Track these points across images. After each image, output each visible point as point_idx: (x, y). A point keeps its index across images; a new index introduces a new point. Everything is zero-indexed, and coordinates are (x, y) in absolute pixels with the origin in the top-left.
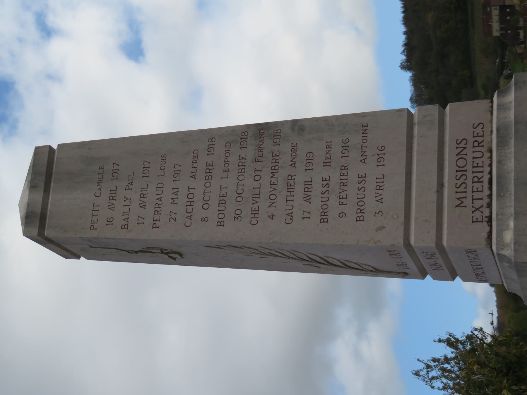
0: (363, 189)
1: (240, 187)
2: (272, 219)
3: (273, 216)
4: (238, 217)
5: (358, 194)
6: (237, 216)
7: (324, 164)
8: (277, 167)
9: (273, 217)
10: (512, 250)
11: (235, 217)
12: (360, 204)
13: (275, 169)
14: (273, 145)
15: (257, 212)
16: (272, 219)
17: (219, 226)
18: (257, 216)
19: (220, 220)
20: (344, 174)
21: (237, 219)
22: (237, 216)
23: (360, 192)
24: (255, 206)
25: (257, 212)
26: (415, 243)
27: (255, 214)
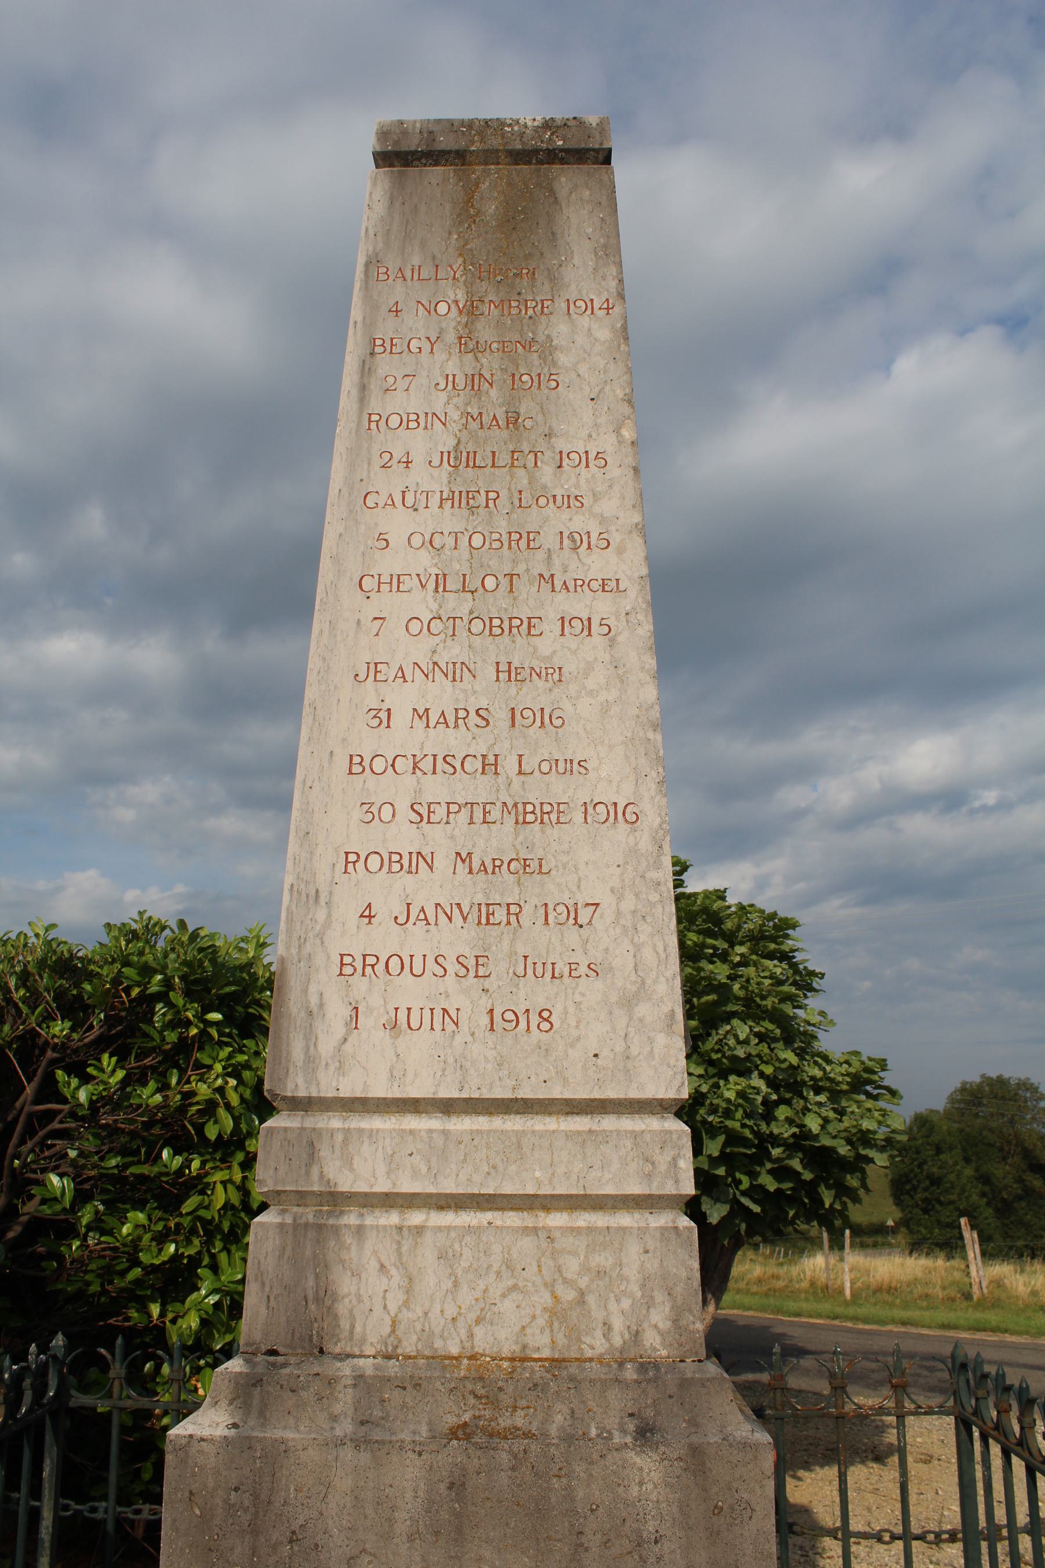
0: (440, 971)
1: (450, 541)
2: (362, 916)
3: (370, 917)
5: (432, 1029)
6: (375, 809)
7: (501, 679)
8: (499, 631)
9: (366, 917)
10: (336, 559)
12: (394, 963)
13: (525, 813)
14: (563, 618)
15: (395, 588)
16: (362, 916)
17: (347, 858)
18: (386, 587)
19: (366, 763)
20: (493, 914)
21: (375, 717)
22: (375, 809)
23: (430, 960)
24: (407, 583)
26: (260, 1223)
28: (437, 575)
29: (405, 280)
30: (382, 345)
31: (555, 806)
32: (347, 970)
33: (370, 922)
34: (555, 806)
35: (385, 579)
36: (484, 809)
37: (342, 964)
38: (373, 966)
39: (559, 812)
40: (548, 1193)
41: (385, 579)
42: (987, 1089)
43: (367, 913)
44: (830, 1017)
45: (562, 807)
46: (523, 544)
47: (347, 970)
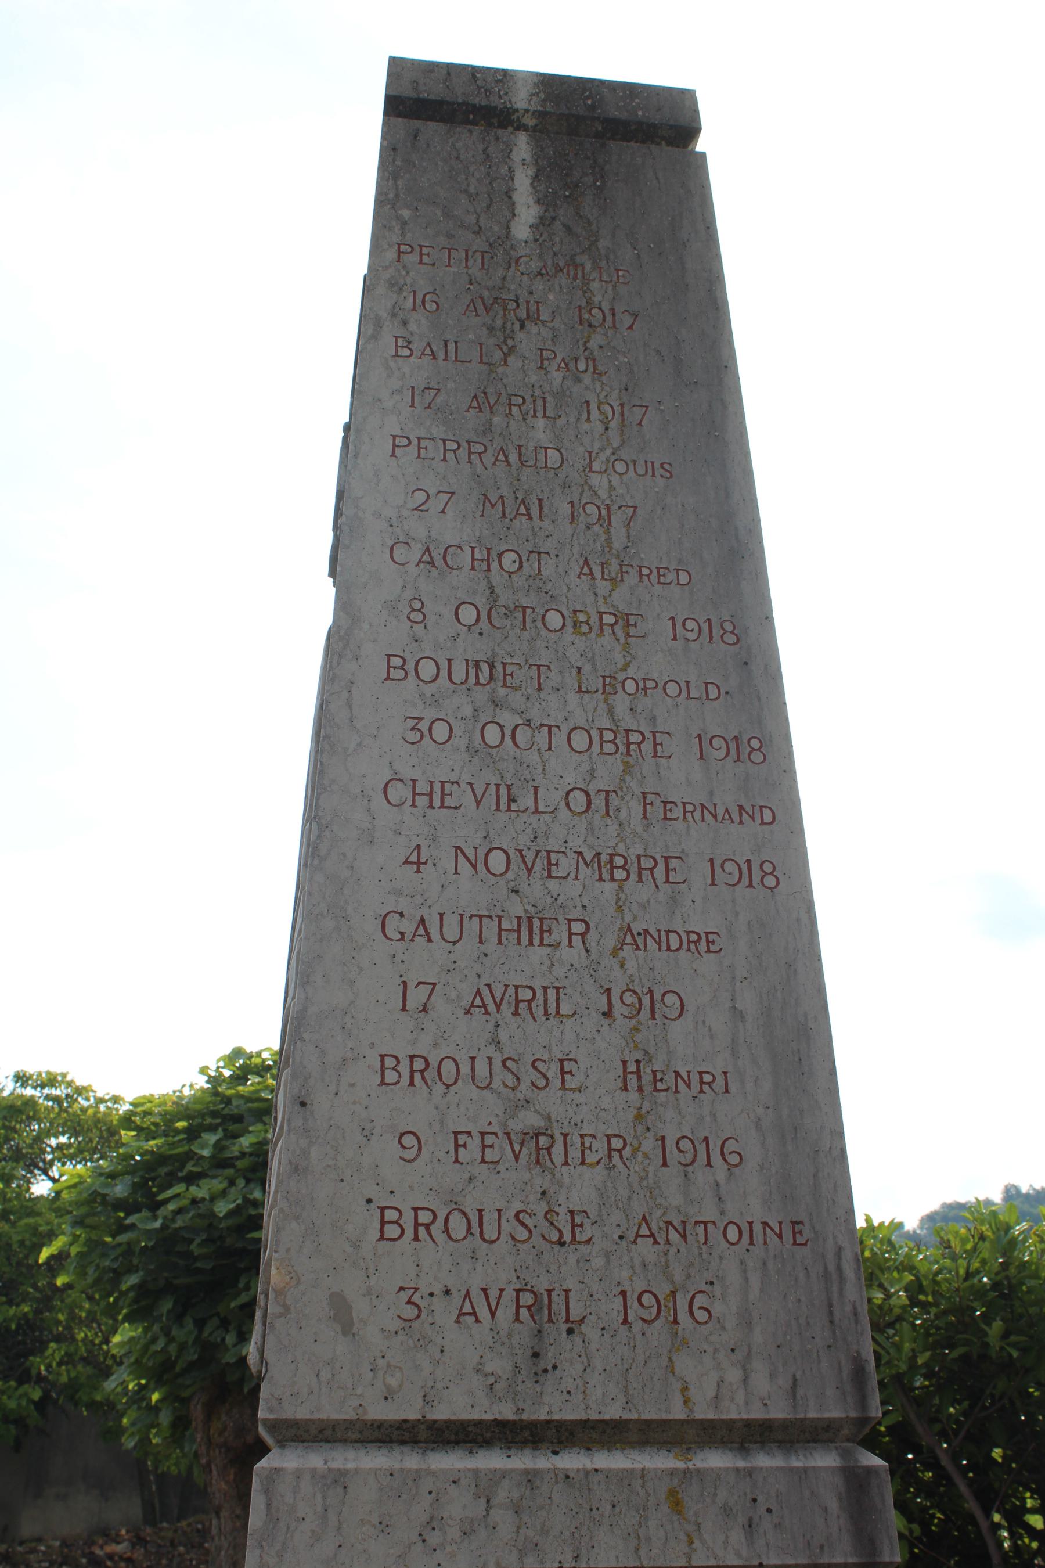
2: (406, 862)
3: (418, 863)
4: (419, 730)
11: (420, 719)
15: (437, 803)
16: (406, 862)
22: (424, 726)
25: (437, 803)
27: (430, 795)
28: (498, 786)
29: (434, 358)
30: (402, 668)
31: (703, 936)
32: (392, 1231)
33: (418, 871)
34: (703, 936)
35: (422, 787)
36: (562, 1068)
37: (383, 1223)
38: (427, 1226)
39: (708, 941)
40: (654, 1416)
41: (422, 787)
42: (1033, 1267)
43: (414, 858)
44: (683, 1399)
45: (711, 937)
46: (654, 577)
47: (392, 1231)
